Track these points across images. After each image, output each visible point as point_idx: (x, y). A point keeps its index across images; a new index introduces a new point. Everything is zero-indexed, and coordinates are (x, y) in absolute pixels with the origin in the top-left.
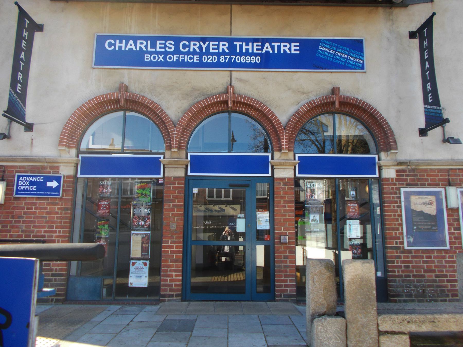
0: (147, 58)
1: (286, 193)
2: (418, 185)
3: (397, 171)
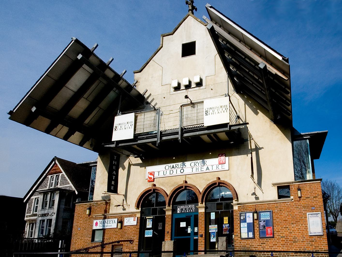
3: (238, 207)
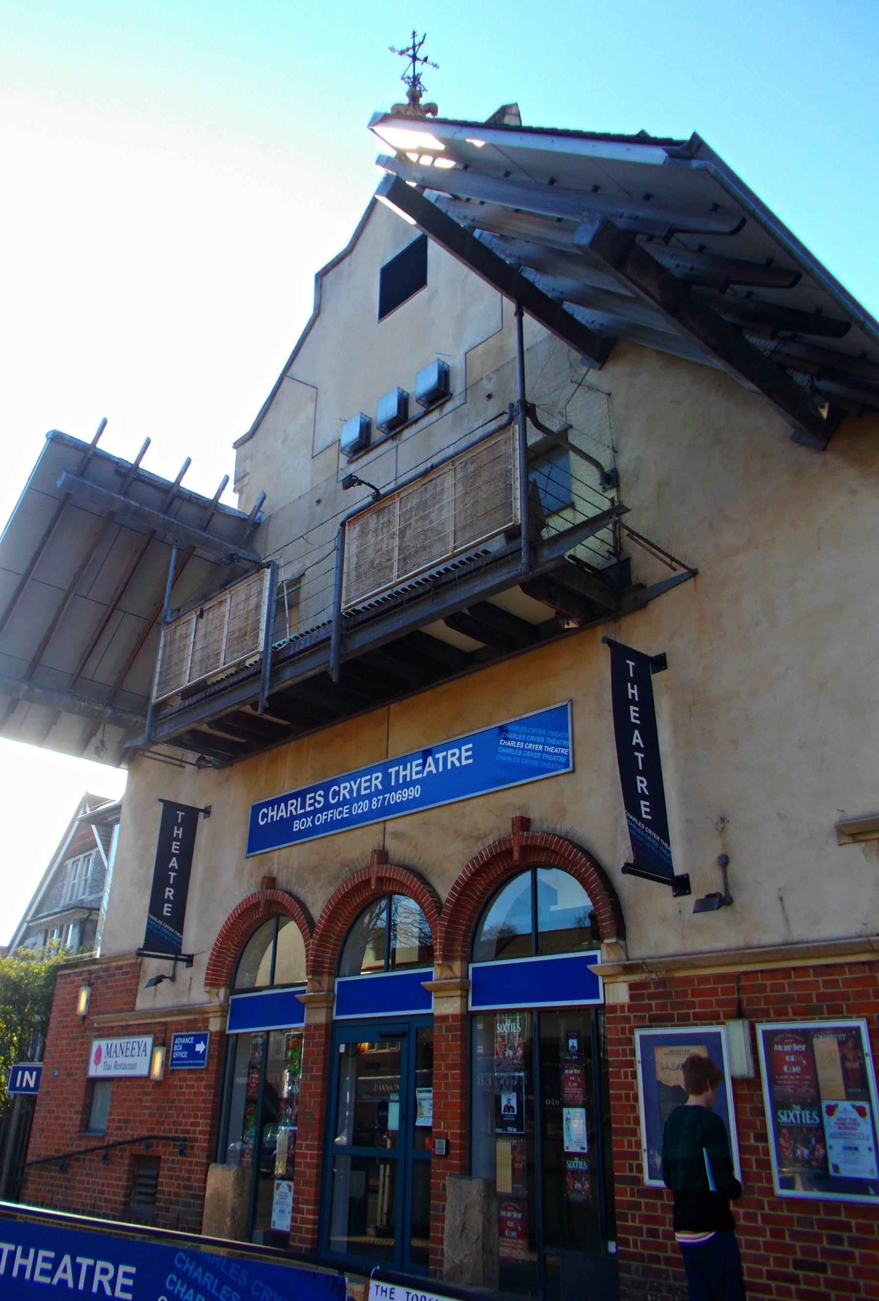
0: (297, 826)
1: (449, 1048)
2: (674, 1021)
3: (632, 986)
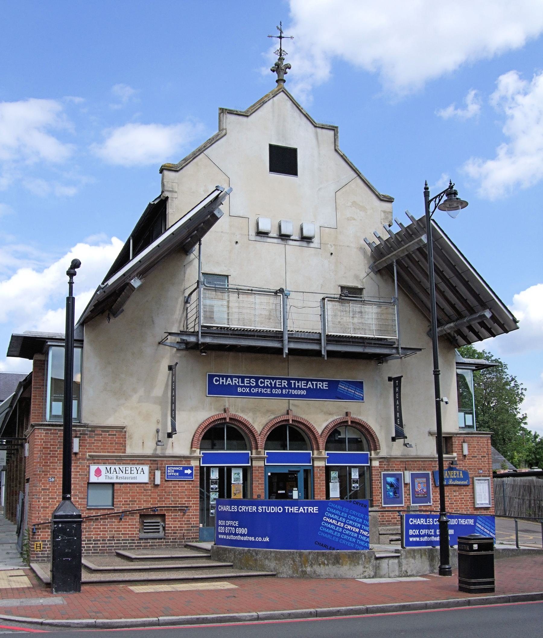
0: (239, 390)
3: (380, 462)
